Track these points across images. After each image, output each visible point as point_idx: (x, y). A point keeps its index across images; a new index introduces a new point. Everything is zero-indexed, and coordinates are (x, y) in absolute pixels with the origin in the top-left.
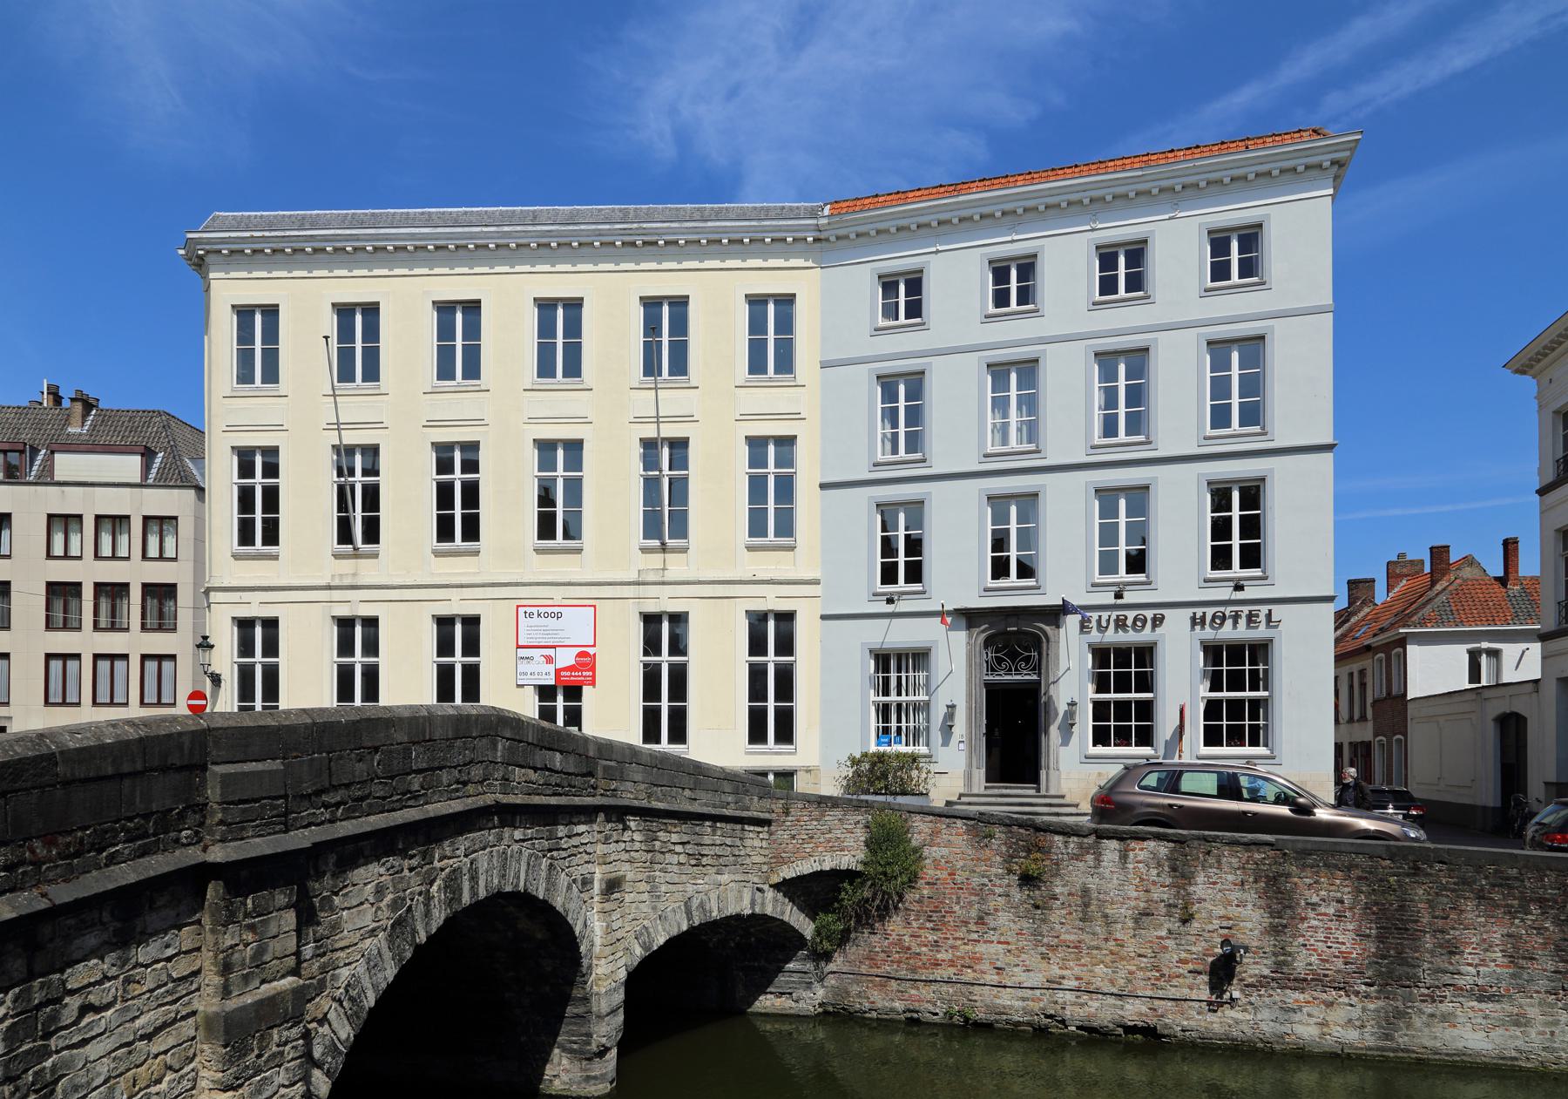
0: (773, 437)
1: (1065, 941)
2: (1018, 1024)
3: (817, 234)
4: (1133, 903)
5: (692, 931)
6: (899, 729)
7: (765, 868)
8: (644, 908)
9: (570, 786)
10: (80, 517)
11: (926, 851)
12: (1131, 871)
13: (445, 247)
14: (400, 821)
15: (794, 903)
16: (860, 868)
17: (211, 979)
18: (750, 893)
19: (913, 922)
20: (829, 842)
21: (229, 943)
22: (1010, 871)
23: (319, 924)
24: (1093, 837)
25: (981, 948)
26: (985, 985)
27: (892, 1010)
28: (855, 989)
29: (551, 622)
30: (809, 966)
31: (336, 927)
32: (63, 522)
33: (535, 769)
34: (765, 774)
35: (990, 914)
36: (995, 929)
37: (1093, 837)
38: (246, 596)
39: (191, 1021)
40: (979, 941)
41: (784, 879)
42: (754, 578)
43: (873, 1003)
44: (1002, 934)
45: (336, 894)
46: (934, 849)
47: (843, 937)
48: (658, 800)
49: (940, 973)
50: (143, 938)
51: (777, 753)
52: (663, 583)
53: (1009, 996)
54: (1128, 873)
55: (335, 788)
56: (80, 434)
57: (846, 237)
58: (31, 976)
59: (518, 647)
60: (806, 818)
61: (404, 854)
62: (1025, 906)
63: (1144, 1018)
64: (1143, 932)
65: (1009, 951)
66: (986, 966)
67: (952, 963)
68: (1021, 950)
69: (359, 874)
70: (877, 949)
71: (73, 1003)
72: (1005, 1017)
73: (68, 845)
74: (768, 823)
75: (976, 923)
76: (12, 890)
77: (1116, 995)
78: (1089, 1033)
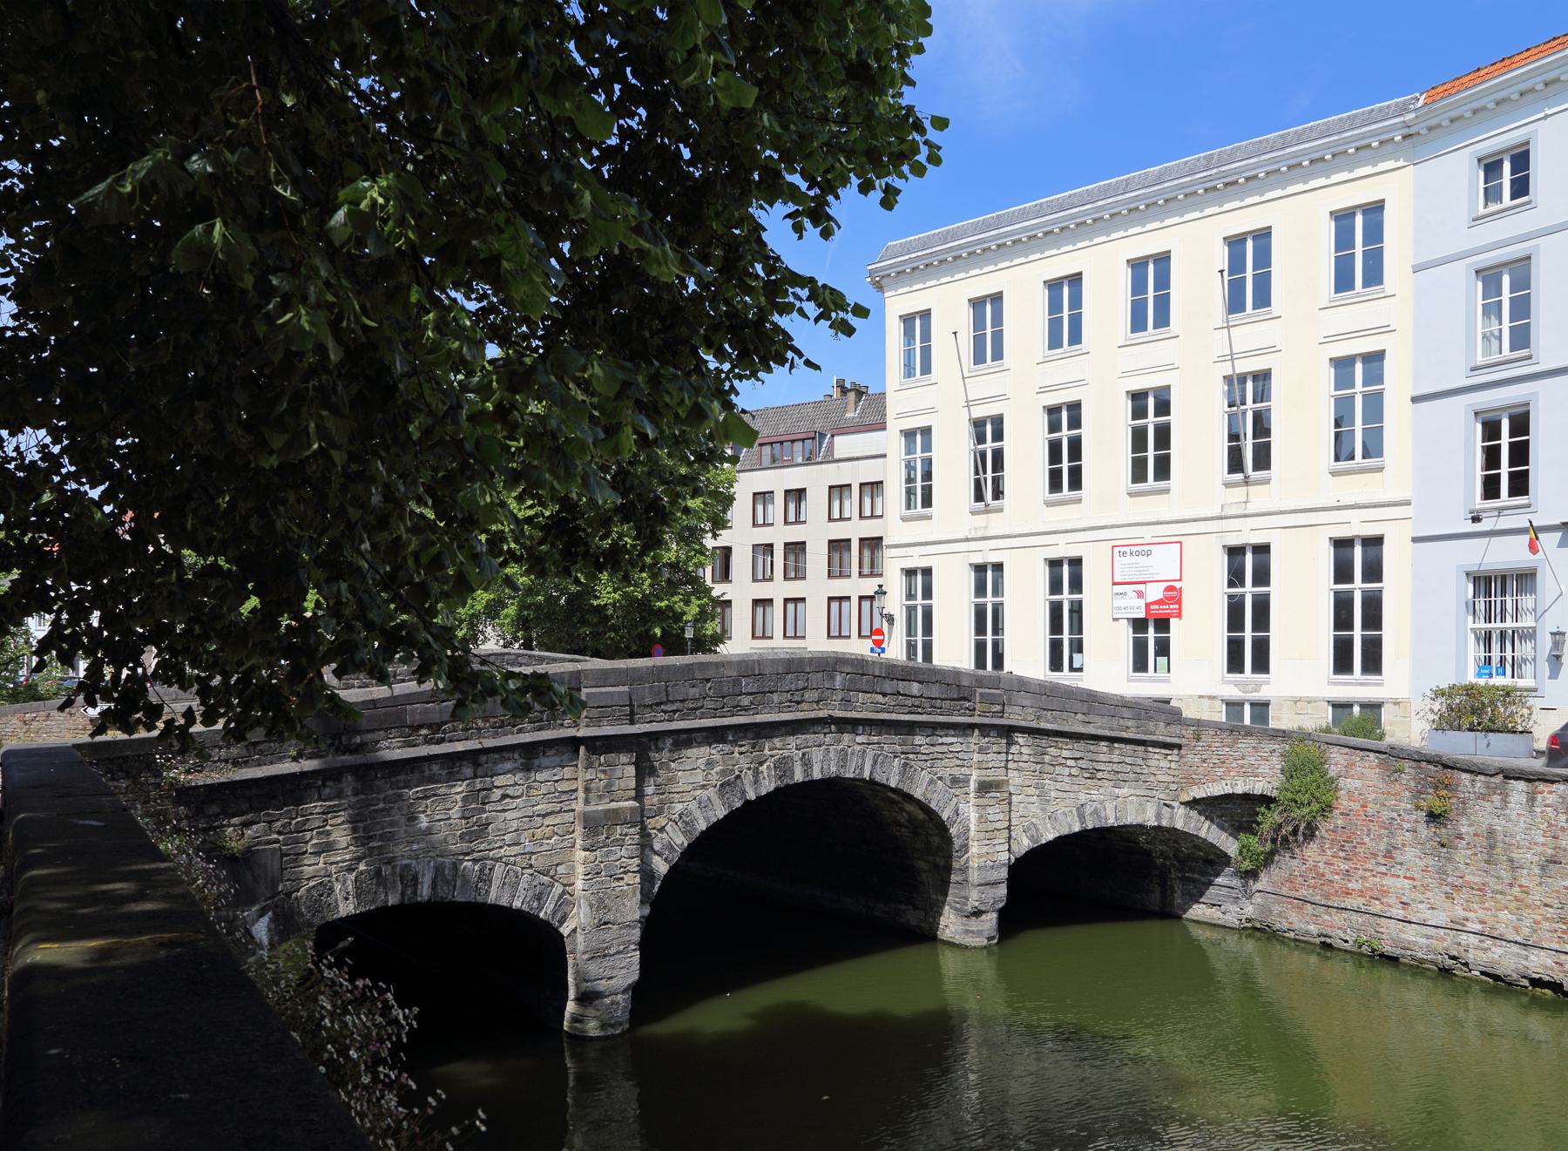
0: (1360, 355)
1: (1469, 882)
2: (1422, 961)
3: (1406, 131)
4: (1539, 849)
5: (1083, 835)
6: (1502, 660)
7: (1173, 787)
8: (1034, 809)
9: (932, 707)
10: (850, 485)
11: (1341, 782)
12: (1539, 815)
13: (1051, 232)
14: (727, 723)
15: (1212, 821)
16: (1275, 794)
17: (581, 794)
18: (1155, 808)
19: (1328, 851)
20: (1242, 767)
21: (589, 777)
22: (1418, 808)
23: (658, 776)
24: (1500, 777)
25: (1388, 881)
26: (1391, 918)
27: (1308, 933)
28: (1276, 908)
29: (1142, 560)
30: (1236, 882)
31: (671, 780)
32: (838, 491)
33: (884, 695)
34: (1349, 706)
35: (1398, 848)
36: (1401, 864)
37: (1500, 777)
38: (910, 551)
39: (571, 814)
40: (1386, 874)
41: (1195, 798)
42: (1338, 504)
43: (1291, 923)
44: (1408, 870)
45: (673, 761)
46: (1349, 780)
47: (1266, 860)
48: (1048, 721)
49: (1354, 902)
50: (540, 768)
51: (1362, 684)
52: (1245, 516)
53: (1414, 933)
54: (1536, 817)
55: (672, 702)
56: (854, 418)
57: (1439, 126)
58: (476, 776)
59: (1114, 584)
60: (1217, 745)
61: (734, 743)
62: (1432, 843)
63: (1550, 972)
64: (1550, 880)
65: (1415, 887)
66: (1392, 900)
67: (1361, 894)
68: (1426, 887)
69: (693, 752)
70: (1296, 873)
71: (497, 793)
72: (1410, 953)
73: (495, 722)
74: (1179, 747)
75: (1385, 856)
76: (466, 739)
77: (1520, 944)
78: (1494, 980)
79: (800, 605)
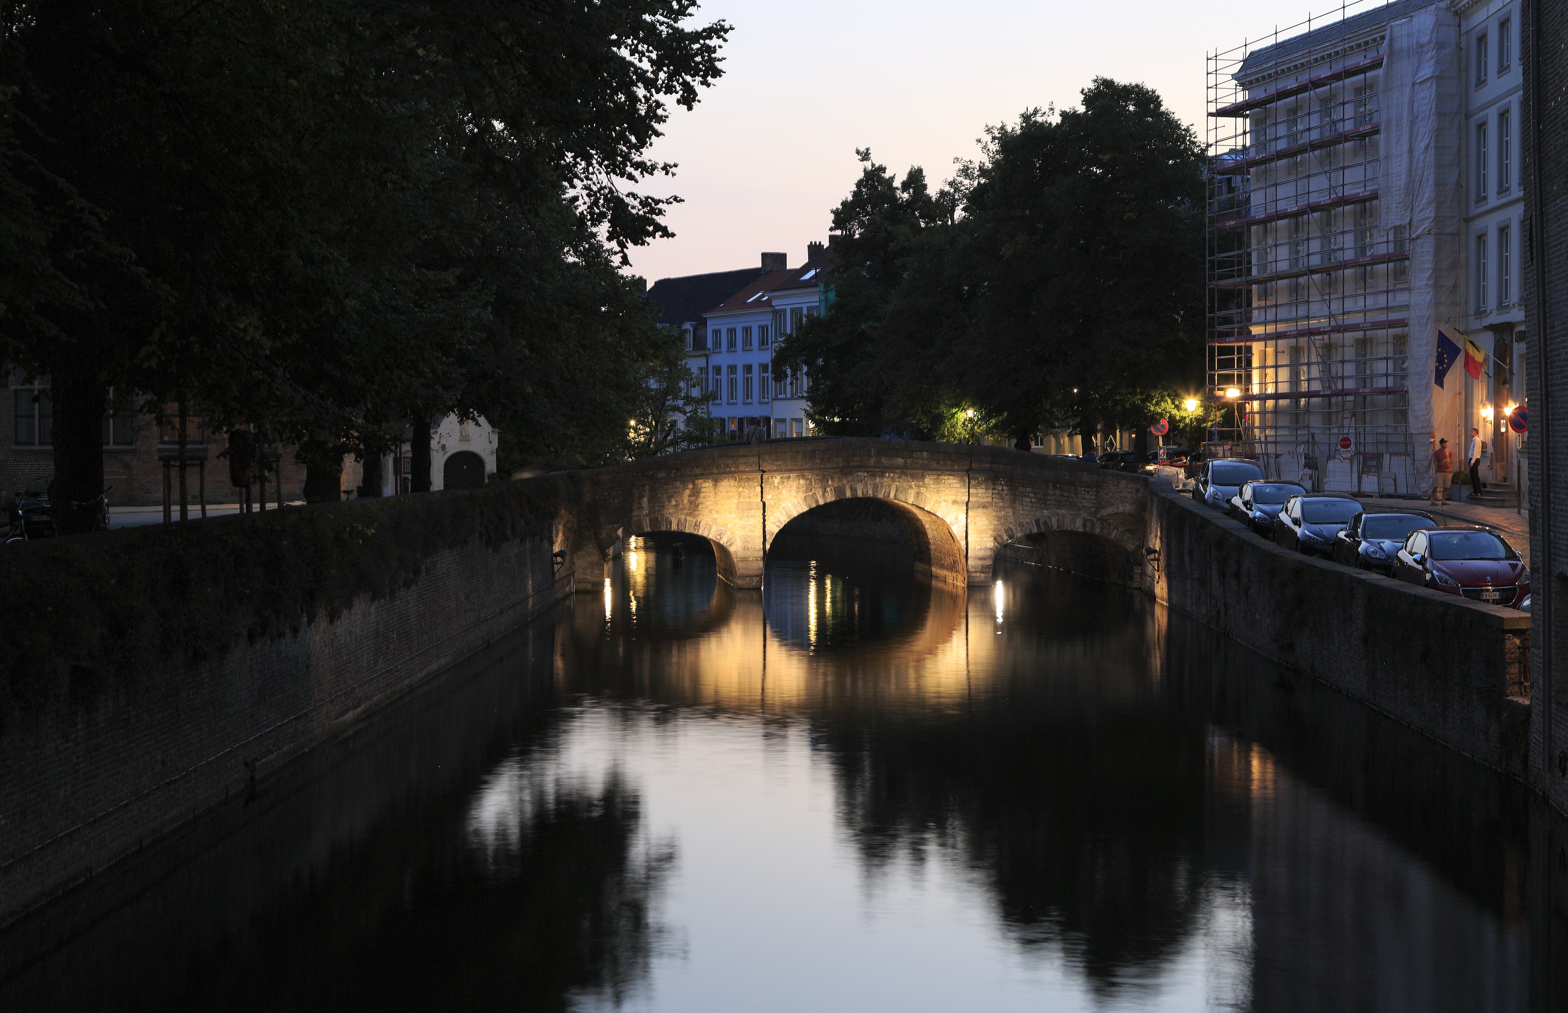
79: (1355, 490)
